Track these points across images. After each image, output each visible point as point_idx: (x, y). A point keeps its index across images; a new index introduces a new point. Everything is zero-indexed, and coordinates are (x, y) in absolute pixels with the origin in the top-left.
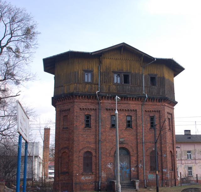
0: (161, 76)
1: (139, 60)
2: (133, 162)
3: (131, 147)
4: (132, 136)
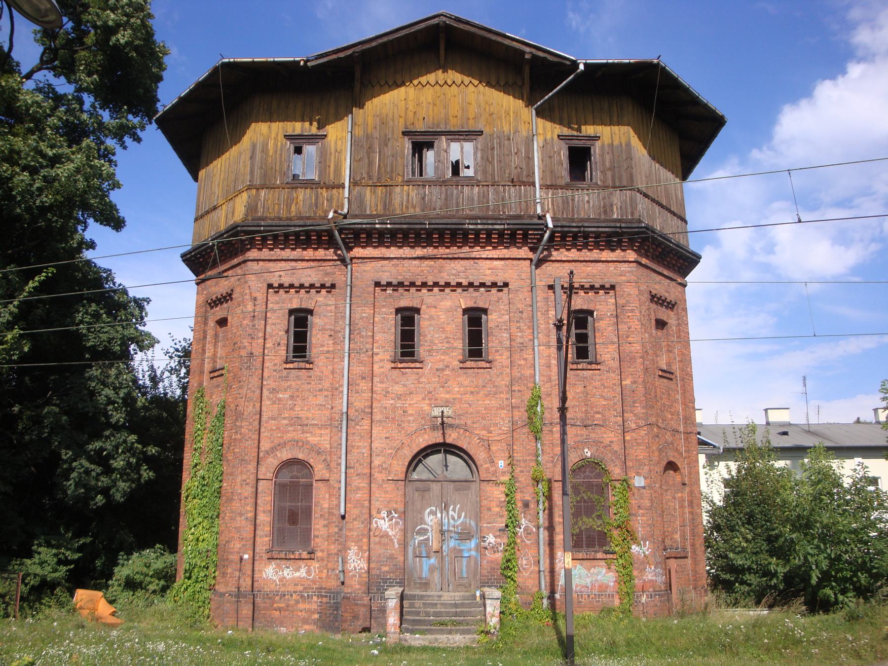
0: (616, 143)
1: (515, 83)
2: (489, 509)
4: (486, 396)
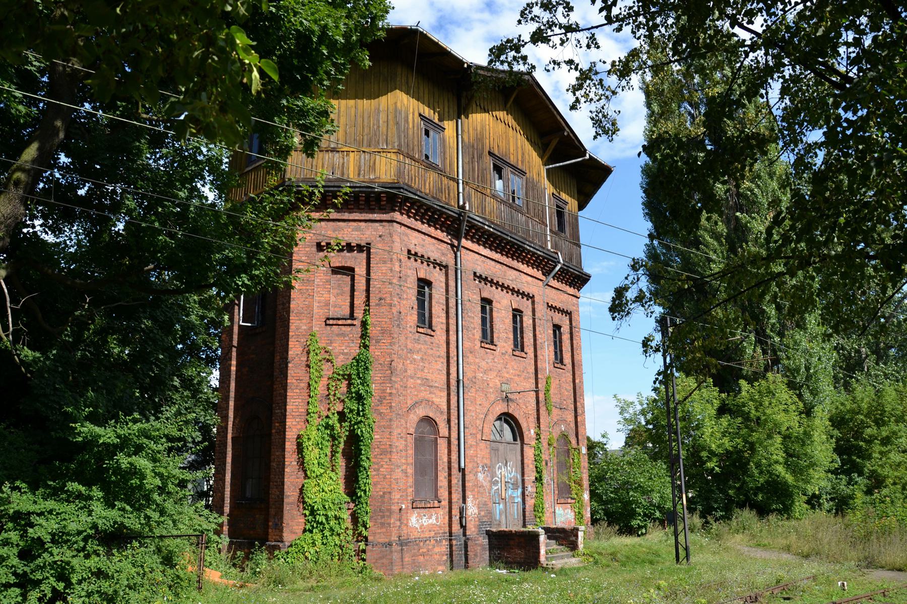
3: (524, 411)
